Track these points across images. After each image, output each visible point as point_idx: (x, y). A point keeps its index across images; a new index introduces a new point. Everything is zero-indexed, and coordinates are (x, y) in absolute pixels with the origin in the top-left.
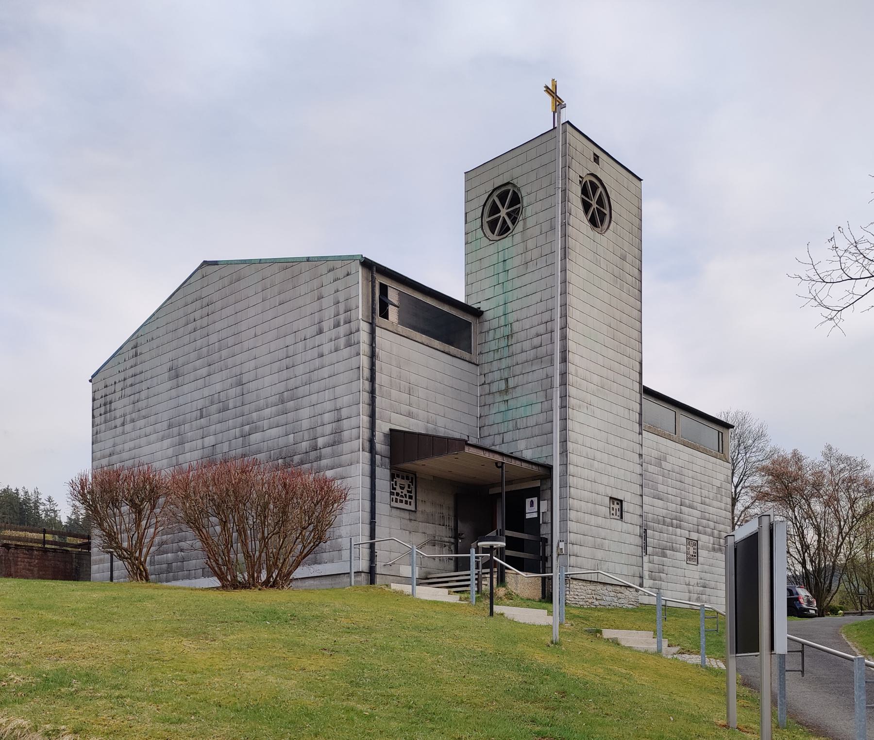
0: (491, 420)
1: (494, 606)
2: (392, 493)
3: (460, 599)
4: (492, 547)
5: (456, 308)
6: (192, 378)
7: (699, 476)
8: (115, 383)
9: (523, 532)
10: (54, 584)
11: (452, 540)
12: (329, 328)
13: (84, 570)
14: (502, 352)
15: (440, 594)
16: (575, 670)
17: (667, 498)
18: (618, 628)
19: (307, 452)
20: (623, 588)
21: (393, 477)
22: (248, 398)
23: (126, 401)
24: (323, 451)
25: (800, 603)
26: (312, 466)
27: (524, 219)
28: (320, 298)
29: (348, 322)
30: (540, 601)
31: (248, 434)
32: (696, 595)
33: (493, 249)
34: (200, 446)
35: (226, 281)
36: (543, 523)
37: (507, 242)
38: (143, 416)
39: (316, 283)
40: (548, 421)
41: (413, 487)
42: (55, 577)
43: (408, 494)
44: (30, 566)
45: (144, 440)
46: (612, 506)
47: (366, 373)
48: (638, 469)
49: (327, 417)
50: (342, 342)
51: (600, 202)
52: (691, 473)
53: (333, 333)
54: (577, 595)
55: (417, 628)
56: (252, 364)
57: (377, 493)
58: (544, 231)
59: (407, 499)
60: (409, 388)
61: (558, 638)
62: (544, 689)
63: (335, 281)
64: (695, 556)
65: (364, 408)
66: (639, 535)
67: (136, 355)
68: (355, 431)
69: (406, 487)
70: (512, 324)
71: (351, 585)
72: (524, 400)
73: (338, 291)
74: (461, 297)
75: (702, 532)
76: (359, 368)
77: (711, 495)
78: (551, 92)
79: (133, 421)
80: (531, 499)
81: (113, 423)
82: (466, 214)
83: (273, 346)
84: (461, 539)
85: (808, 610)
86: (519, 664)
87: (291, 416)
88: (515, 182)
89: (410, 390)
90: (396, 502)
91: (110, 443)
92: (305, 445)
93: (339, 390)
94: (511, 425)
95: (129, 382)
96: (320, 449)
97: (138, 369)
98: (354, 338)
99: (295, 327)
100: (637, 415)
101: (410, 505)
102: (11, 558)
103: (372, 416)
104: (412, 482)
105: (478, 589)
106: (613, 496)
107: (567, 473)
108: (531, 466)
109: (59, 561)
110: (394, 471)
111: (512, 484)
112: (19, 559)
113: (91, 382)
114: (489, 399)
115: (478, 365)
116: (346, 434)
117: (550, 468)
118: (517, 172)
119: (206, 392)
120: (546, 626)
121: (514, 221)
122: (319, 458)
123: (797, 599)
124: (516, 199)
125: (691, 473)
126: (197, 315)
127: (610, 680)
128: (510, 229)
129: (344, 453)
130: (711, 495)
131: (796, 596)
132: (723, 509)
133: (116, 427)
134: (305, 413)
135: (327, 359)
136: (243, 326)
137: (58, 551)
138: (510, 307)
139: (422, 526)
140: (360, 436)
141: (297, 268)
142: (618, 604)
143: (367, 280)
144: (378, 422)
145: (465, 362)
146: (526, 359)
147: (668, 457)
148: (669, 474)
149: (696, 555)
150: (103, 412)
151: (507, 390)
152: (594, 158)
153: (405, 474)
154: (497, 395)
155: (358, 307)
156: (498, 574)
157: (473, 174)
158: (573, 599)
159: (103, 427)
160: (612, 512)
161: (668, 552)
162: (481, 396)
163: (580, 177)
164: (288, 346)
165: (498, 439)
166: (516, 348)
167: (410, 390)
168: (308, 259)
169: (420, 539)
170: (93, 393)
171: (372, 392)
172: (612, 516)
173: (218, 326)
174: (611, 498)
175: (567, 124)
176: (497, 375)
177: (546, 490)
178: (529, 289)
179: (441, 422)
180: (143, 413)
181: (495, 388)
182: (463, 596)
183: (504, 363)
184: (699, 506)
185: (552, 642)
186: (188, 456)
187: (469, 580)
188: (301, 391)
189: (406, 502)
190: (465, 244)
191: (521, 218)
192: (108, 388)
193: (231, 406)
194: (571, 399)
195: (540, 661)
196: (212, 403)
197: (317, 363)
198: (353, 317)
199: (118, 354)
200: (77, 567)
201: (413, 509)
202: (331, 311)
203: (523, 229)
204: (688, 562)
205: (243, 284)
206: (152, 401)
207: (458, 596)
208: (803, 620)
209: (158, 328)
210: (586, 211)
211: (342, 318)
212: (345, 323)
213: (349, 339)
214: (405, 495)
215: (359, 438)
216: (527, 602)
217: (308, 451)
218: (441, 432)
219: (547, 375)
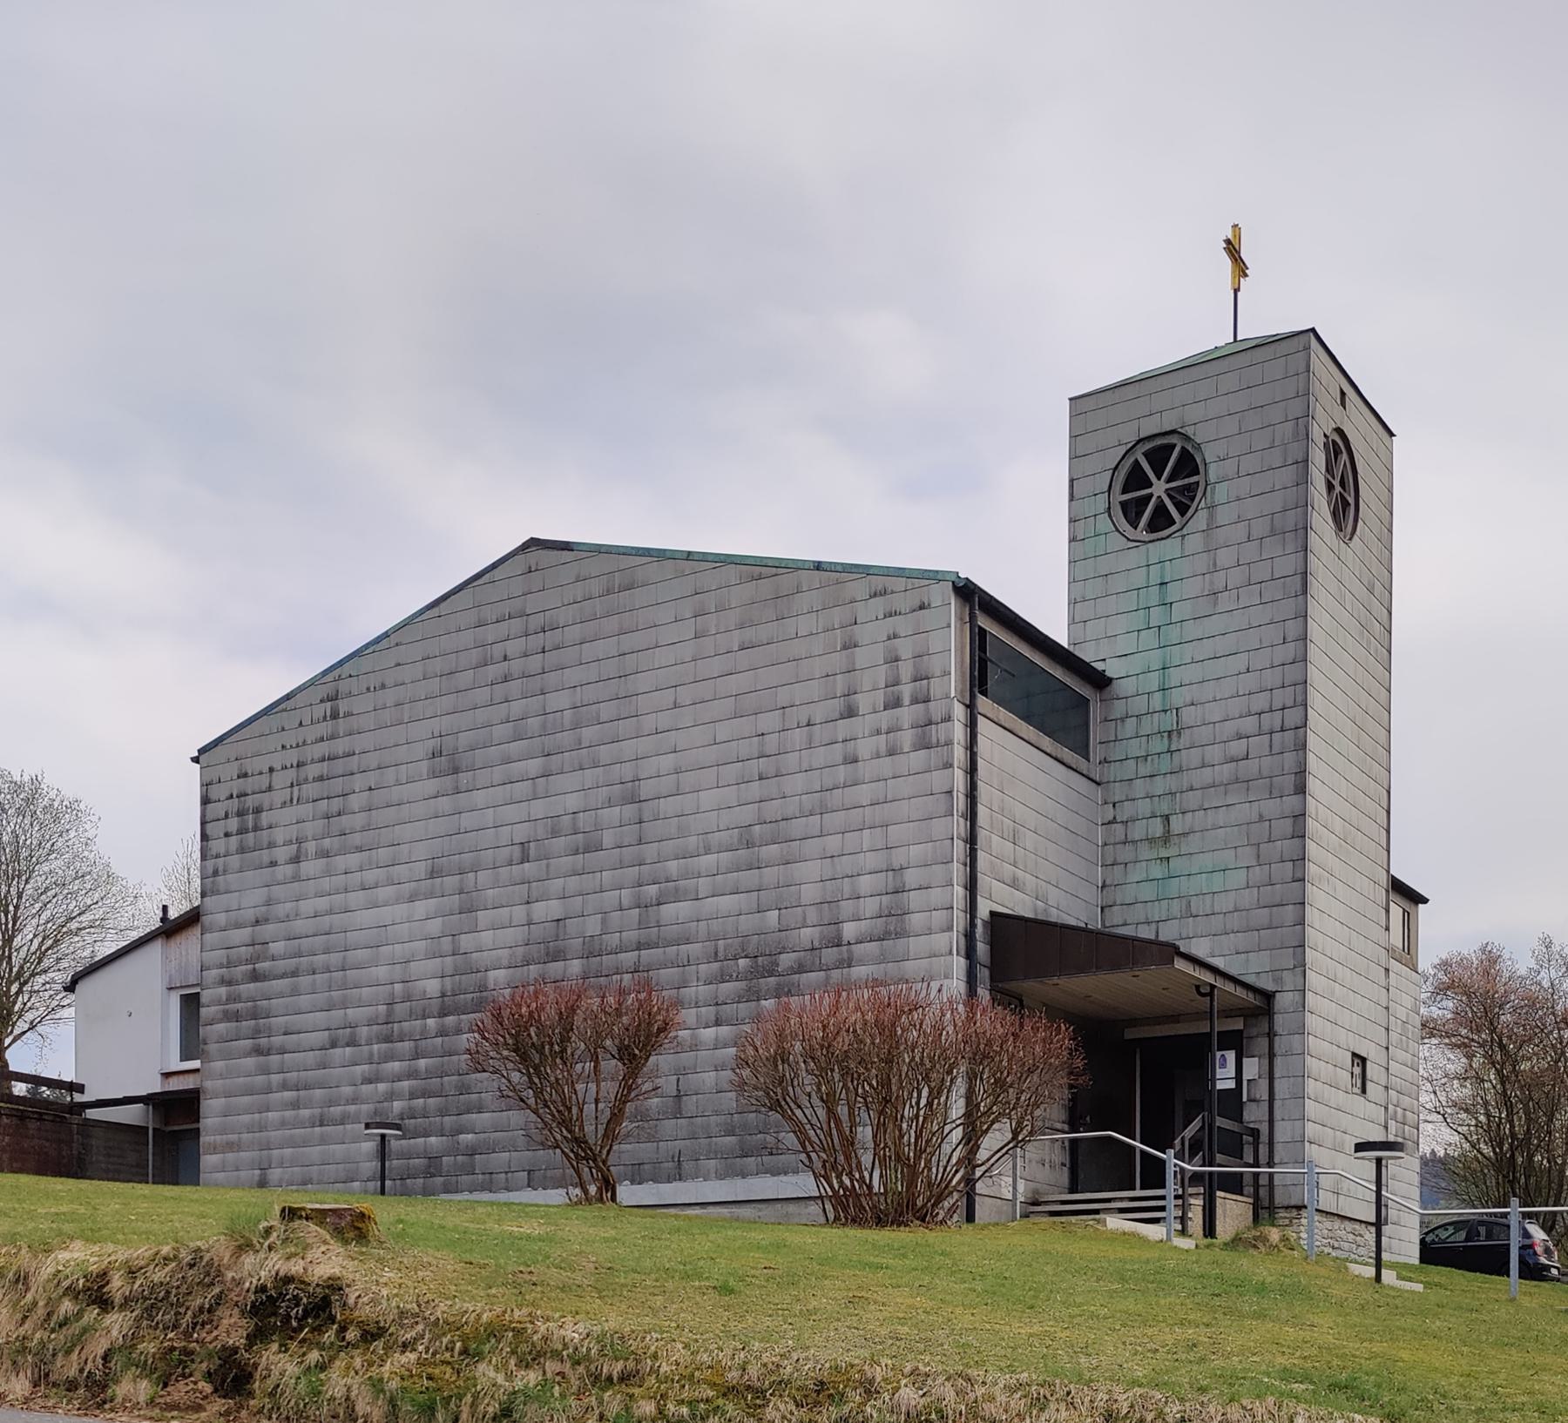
0: (1129, 893)
1: (1383, 1271)
5: (1068, 669)
6: (497, 779)
8: (271, 770)
10: (60, 1187)
12: (874, 708)
13: (94, 1159)
14: (1156, 761)
23: (305, 810)
24: (858, 950)
25: (1535, 1253)
26: (828, 978)
27: (1211, 508)
28: (850, 645)
31: (654, 902)
33: (1136, 557)
35: (595, 587)
36: (1250, 1100)
37: (1168, 547)
38: (357, 848)
39: (837, 615)
40: (1262, 904)
42: (41, 1170)
45: (357, 898)
47: (960, 802)
50: (907, 738)
56: (667, 762)
58: (1255, 534)
65: (958, 871)
70: (1180, 710)
72: (1206, 861)
73: (895, 637)
76: (950, 792)
78: (1232, 249)
79: (325, 854)
81: (265, 856)
82: (1072, 481)
83: (724, 730)
85: (1547, 1268)
87: (770, 875)
88: (1189, 431)
92: (807, 935)
94: (1176, 907)
95: (312, 770)
97: (340, 746)
99: (783, 696)
103: (972, 886)
105: (1183, 1227)
107: (1304, 1007)
113: (198, 762)
114: (1125, 853)
115: (1098, 784)
116: (916, 920)
119: (538, 808)
121: (1183, 509)
124: (1189, 464)
129: (912, 955)
133: (273, 864)
134: (809, 871)
135: (866, 769)
136: (642, 682)
137: (46, 1117)
138: (1175, 676)
140: (953, 926)
141: (787, 581)
143: (961, 619)
146: (1211, 781)
151: (1166, 838)
155: (947, 673)
156: (1204, 1199)
157: (1090, 404)
162: (1106, 844)
164: (763, 734)
166: (1191, 757)
168: (819, 566)
170: (202, 785)
171: (972, 840)
173: (573, 676)
174: (1354, 1055)
175: (1311, 334)
176: (1144, 807)
177: (1257, 1036)
178: (1221, 645)
179: (1054, 896)
180: (357, 839)
181: (1137, 831)
183: (1160, 785)
186: (487, 937)
187: (1162, 1209)
188: (797, 827)
190: (1070, 542)
191: (1202, 504)
192: (250, 779)
193: (608, 838)
196: (555, 833)
197: (842, 773)
199: (280, 707)
200: (80, 1153)
202: (881, 675)
203: (1208, 525)
205: (639, 596)
206: (380, 816)
208: (1492, 1282)
211: (906, 691)
212: (915, 701)
213: (924, 733)
217: (816, 944)
218: (1054, 916)
219: (1261, 816)
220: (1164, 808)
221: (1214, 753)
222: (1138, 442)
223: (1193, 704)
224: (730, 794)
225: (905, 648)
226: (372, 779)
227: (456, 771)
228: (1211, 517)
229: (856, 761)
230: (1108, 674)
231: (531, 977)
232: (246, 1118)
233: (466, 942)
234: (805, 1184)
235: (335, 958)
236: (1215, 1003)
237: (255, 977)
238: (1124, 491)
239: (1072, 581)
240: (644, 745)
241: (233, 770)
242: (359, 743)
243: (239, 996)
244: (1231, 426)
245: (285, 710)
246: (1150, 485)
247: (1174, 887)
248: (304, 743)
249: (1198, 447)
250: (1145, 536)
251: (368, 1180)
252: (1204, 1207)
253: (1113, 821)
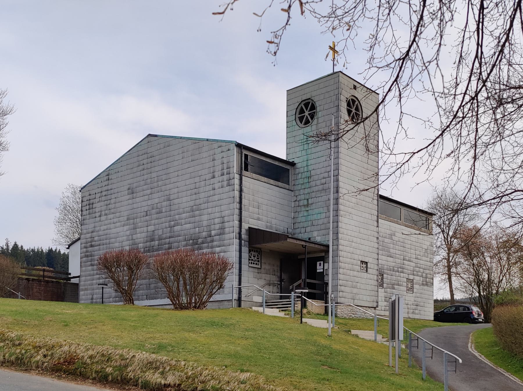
0: (299, 220)
2: (249, 260)
3: (285, 315)
4: (302, 292)
7: (414, 244)
8: (96, 193)
9: (315, 280)
11: (279, 283)
15: (274, 312)
16: (336, 346)
17: (396, 256)
18: (360, 329)
19: (205, 238)
20: (367, 308)
21: (250, 251)
22: (173, 207)
23: (102, 203)
25: (473, 315)
26: (208, 245)
27: (318, 118)
28: (214, 160)
29: (228, 173)
30: (324, 315)
32: (412, 310)
33: (301, 131)
34: (145, 231)
35: (162, 146)
36: (326, 275)
39: (211, 152)
41: (260, 256)
43: (257, 260)
44: (39, 290)
45: (112, 226)
46: (362, 265)
47: (238, 200)
48: (376, 245)
49: (217, 221)
50: (225, 183)
51: (357, 109)
52: (409, 242)
54: (343, 312)
55: (272, 329)
56: (176, 190)
57: (243, 260)
59: (257, 262)
60: (258, 205)
61: (331, 334)
62: (324, 353)
63: (222, 152)
64: (411, 288)
65: (236, 217)
66: (376, 280)
67: (108, 180)
68: (231, 229)
69: (256, 256)
71: (232, 307)
72: (316, 211)
73: (223, 158)
74: (284, 157)
75: (416, 275)
76: (234, 197)
77: (422, 254)
79: (106, 215)
80: (319, 262)
81: (94, 215)
83: (188, 182)
84: (283, 282)
85: (478, 319)
86: (315, 344)
87: (197, 218)
88: (313, 98)
89: (258, 207)
90: (251, 264)
91: (92, 225)
94: (310, 223)
95: (104, 193)
96: (213, 236)
97: (109, 187)
98: (231, 182)
100: (376, 217)
101: (258, 265)
102: (30, 286)
103: (240, 221)
104: (259, 253)
106: (362, 260)
108: (320, 246)
109: (54, 288)
110: (250, 248)
111: (310, 254)
112: (34, 287)
114: (299, 209)
115: (292, 191)
116: (227, 230)
117: (328, 246)
118: (314, 94)
119: (150, 202)
120: (326, 329)
121: (312, 118)
122: (212, 241)
123: (472, 313)
124: (313, 107)
125: (409, 242)
126: (145, 162)
127: (350, 350)
128: (310, 122)
130: (422, 254)
131: (471, 311)
132: (429, 261)
133: (96, 217)
134: (205, 217)
135: (217, 191)
136: (171, 170)
138: (310, 162)
139: (264, 276)
141: (201, 144)
142: (364, 316)
143: (239, 153)
144: (243, 224)
145: (286, 190)
147: (397, 234)
148: (397, 243)
149: (412, 288)
150: (88, 209)
151: (308, 205)
152: (354, 87)
153: (256, 250)
154: (303, 207)
155: (234, 167)
158: (341, 314)
159: (88, 217)
160: (362, 268)
161: (396, 286)
163: (346, 98)
165: (303, 230)
166: (313, 183)
167: (258, 207)
168: (207, 140)
169: (262, 282)
171: (241, 209)
172: (362, 271)
173: (157, 169)
174: (361, 261)
176: (302, 197)
178: (320, 154)
179: (274, 221)
180: (112, 211)
181: (301, 203)
182: (287, 312)
183: (307, 191)
184: (414, 260)
185: (328, 336)
186: (139, 235)
187: (290, 304)
188: (203, 206)
189: (256, 264)
191: (316, 118)
193: (164, 211)
194: (341, 211)
195: (323, 343)
196: (153, 209)
197: (212, 192)
198: (231, 172)
199: (98, 177)
200: (63, 291)
201: (260, 267)
202: (220, 167)
204: (408, 292)
207: (283, 313)
209: (121, 166)
210: (349, 115)
211: (225, 171)
212: (227, 174)
214: (256, 260)
215: (234, 232)
216: (317, 316)
217: (206, 237)
220: (307, 197)
221: (318, 182)
222: (302, 101)
223: (313, 170)
224: (189, 198)
225: (225, 160)
226: (116, 195)
227: (133, 193)
228: (318, 121)
229: (215, 189)
230: (295, 162)
231: (148, 245)
232: (89, 282)
233: (135, 237)
234: (167, 301)
235: (108, 241)
236: (306, 250)
237: (92, 246)
238: (299, 114)
239: (287, 138)
240: (171, 186)
241: (88, 193)
242: (114, 186)
243: (88, 251)
244: (322, 97)
245: (98, 178)
246: (305, 112)
247: (310, 218)
248: (102, 187)
249: (315, 102)
250: (304, 126)
251: (114, 298)
252: (301, 303)
253: (296, 201)
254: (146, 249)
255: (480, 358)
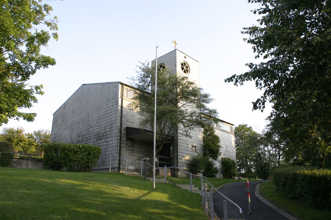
21: (127, 140)
24: (108, 133)
45: (64, 130)
51: (187, 67)
53: (112, 101)
59: (131, 147)
69: (131, 143)
87: (100, 123)
92: (103, 132)
93: (112, 116)
97: (64, 112)
118: (164, 61)
122: (106, 135)
168: (107, 83)
172: (193, 151)
174: (192, 146)
187: (140, 171)
189: (131, 147)
218: (138, 128)
254: (76, 141)
255: (264, 201)
